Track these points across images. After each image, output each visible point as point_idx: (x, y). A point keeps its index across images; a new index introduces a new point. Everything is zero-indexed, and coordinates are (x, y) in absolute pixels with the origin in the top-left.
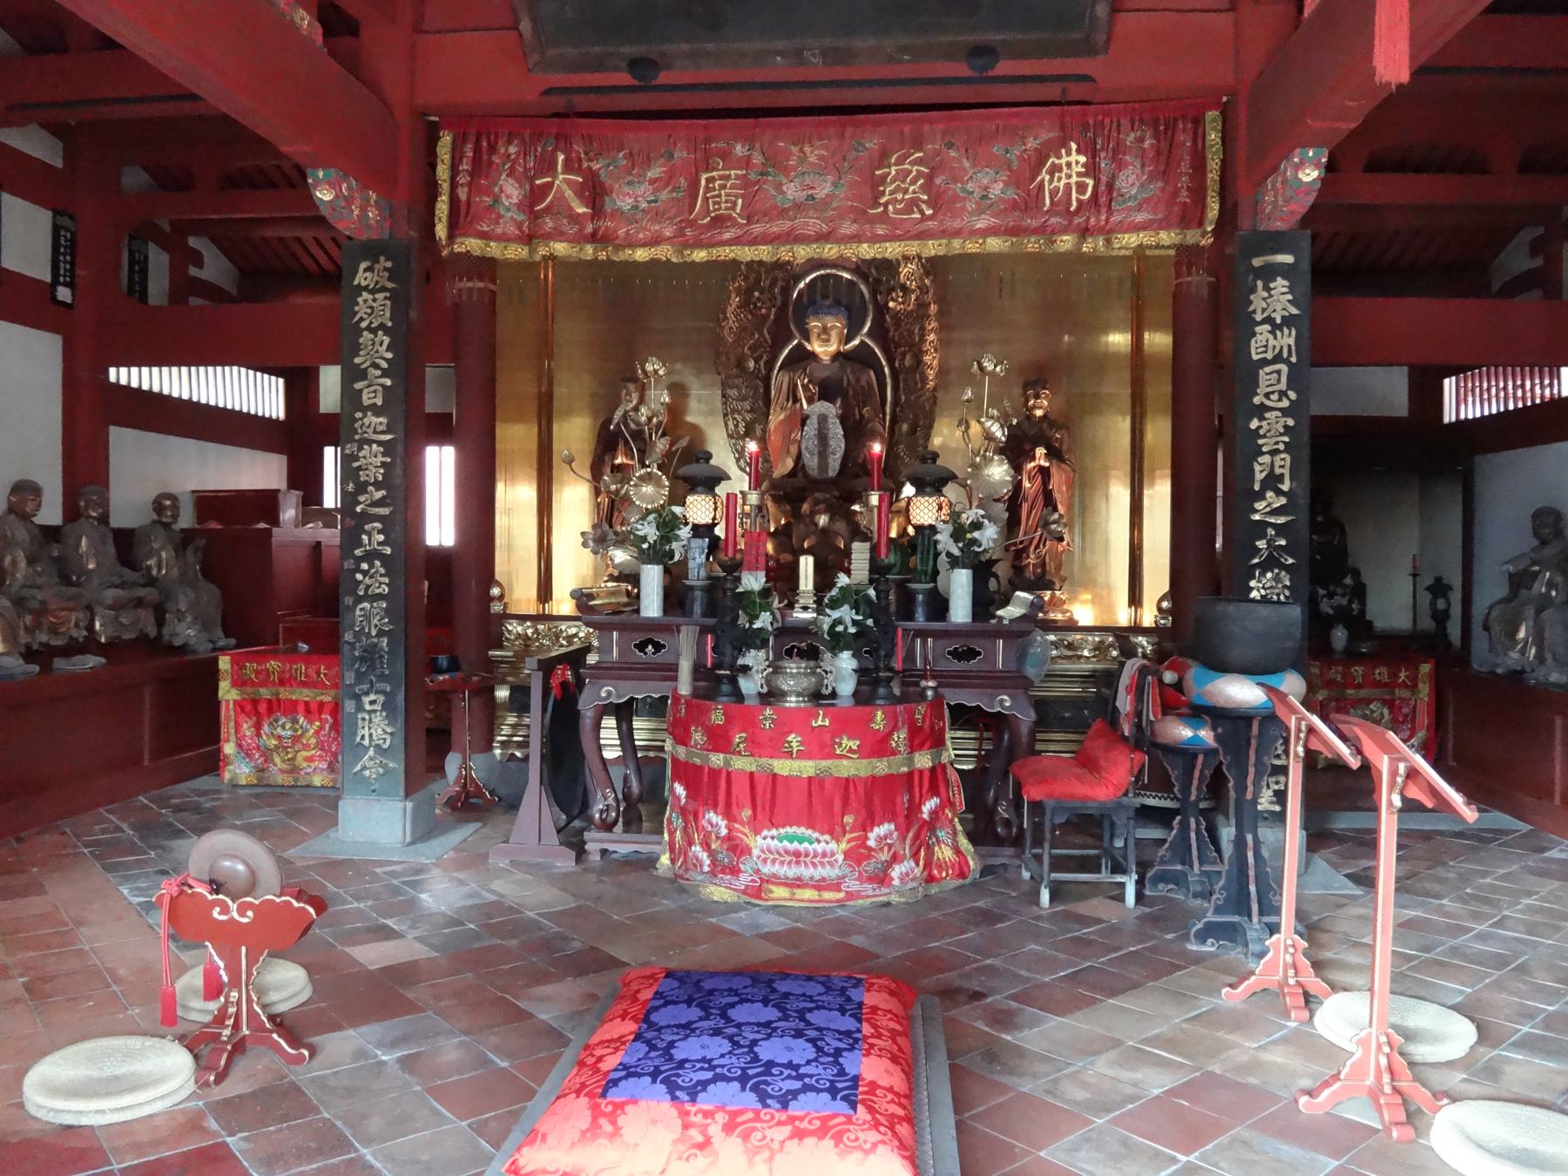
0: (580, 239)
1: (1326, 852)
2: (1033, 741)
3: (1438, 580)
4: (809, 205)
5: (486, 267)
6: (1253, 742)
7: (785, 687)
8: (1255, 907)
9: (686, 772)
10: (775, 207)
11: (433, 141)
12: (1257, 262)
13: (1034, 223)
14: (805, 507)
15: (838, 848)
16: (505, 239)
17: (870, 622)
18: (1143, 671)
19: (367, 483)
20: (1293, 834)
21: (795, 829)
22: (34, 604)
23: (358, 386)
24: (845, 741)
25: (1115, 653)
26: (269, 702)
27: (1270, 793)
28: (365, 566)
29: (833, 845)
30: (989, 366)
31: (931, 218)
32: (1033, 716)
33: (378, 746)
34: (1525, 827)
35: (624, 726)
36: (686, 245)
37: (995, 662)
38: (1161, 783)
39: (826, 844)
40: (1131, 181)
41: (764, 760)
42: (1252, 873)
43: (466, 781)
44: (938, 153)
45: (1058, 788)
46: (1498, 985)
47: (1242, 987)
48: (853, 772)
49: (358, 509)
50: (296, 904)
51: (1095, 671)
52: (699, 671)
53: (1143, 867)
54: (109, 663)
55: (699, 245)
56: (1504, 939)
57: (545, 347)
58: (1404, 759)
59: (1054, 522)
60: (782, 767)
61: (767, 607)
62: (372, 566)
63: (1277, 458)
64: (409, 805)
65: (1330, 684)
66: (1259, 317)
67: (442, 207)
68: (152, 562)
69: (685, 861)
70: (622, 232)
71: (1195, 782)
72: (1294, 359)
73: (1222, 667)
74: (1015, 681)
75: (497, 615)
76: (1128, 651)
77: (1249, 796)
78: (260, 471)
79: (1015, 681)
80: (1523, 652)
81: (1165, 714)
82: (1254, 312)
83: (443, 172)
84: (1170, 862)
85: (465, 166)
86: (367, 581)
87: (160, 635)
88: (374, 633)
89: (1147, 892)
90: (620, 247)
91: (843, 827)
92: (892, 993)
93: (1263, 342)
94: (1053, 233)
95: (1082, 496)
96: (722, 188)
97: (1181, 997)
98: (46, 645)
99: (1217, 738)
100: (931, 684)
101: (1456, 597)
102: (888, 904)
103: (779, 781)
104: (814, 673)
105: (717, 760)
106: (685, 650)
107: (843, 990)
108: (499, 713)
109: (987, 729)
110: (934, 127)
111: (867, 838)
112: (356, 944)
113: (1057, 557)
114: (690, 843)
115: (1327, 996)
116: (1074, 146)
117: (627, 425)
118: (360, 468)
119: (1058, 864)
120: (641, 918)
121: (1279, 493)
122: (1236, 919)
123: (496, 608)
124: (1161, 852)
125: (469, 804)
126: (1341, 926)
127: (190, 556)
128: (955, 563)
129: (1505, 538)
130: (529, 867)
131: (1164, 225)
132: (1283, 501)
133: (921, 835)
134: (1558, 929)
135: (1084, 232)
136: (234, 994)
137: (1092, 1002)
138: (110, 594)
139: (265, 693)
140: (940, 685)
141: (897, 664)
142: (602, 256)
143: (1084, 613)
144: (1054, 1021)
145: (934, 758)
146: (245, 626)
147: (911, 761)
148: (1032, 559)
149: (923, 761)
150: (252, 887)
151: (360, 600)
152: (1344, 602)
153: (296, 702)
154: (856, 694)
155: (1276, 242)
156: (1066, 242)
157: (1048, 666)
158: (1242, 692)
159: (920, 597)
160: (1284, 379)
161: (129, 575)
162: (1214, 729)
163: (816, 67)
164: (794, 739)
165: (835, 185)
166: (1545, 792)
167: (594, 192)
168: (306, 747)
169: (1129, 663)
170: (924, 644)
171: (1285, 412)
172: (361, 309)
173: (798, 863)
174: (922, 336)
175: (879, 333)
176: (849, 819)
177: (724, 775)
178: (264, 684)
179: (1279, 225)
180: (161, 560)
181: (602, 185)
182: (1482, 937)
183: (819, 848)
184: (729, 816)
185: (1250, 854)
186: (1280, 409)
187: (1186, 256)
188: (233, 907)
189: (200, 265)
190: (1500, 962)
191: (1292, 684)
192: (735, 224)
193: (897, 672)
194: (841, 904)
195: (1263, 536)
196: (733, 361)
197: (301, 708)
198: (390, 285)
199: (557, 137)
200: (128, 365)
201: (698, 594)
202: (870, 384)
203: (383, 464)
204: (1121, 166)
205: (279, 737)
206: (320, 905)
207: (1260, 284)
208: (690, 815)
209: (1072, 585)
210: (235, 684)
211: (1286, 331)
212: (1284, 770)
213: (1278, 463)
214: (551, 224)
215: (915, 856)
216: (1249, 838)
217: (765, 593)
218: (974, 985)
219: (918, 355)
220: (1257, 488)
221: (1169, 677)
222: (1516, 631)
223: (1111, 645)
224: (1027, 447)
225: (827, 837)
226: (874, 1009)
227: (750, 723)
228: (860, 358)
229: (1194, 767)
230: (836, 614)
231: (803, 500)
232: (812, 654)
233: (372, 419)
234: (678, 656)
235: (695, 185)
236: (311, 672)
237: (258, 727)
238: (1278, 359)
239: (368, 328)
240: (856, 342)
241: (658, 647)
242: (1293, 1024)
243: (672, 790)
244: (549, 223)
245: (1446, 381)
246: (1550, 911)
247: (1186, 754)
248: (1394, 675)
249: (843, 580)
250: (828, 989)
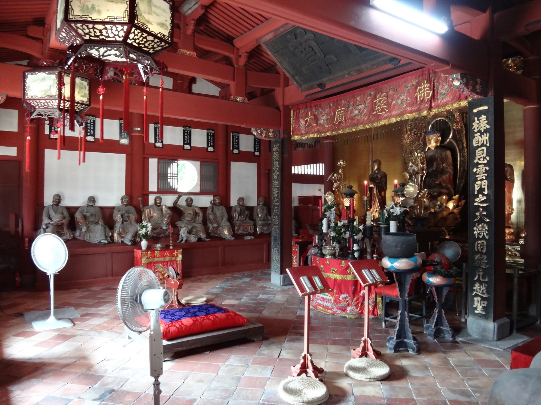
12: (475, 111)
27: (481, 307)
29: (331, 298)
63: (483, 182)
64: (282, 276)
66: (476, 131)
72: (488, 145)
82: (474, 129)
96: (339, 115)
98: (242, 233)
111: (339, 297)
121: (484, 195)
132: (485, 198)
159: (383, 229)
163: (356, 76)
171: (485, 165)
183: (328, 297)
186: (484, 164)
195: (478, 211)
207: (476, 118)
211: (485, 134)
213: (483, 183)
215: (356, 306)
220: (476, 193)
238: (483, 145)
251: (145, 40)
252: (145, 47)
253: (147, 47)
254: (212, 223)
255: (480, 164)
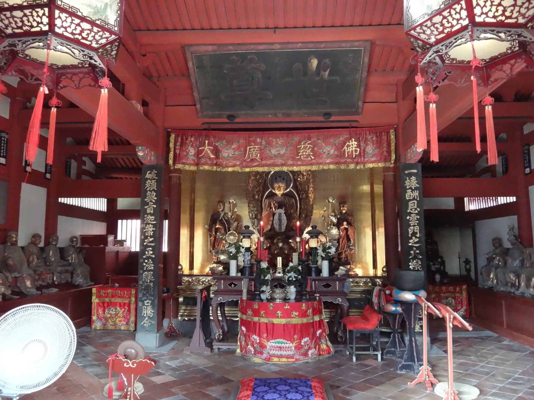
0: (212, 165)
1: (437, 344)
2: (348, 312)
3: (467, 259)
4: (276, 155)
5: (179, 171)
6: (413, 311)
7: (276, 297)
8: (416, 360)
9: (244, 323)
10: (269, 156)
11: (169, 136)
12: (406, 172)
13: (343, 161)
14: (275, 241)
15: (292, 345)
16: (190, 164)
17: (300, 277)
18: (380, 291)
19: (148, 236)
20: (426, 339)
21: (280, 340)
22: (38, 272)
23: (146, 207)
24: (294, 313)
25: (370, 284)
26: (108, 302)
27: (419, 326)
28: (146, 261)
29: (291, 345)
30: (331, 201)
31: (314, 159)
32: (348, 304)
33: (149, 317)
34: (496, 335)
35: (222, 310)
36: (243, 167)
37: (336, 289)
38: (386, 324)
39: (289, 344)
40: (370, 149)
41: (270, 319)
42: (414, 349)
43: (171, 328)
44: (315, 142)
45: (357, 325)
46: (487, 380)
47: (413, 382)
48: (296, 322)
49: (145, 244)
50: (149, 361)
51: (364, 290)
52: (249, 292)
53: (382, 350)
54: (59, 290)
55: (247, 167)
56: (488, 367)
57: (193, 191)
58: (452, 314)
59: (352, 246)
60: (276, 321)
61: (269, 273)
62: (148, 261)
63: (415, 227)
64: (158, 335)
65: (436, 292)
66: (408, 187)
67: (171, 155)
68: (69, 258)
69: (246, 351)
70: (224, 163)
71: (397, 323)
72: (418, 199)
73: (403, 289)
74: (342, 294)
75: (180, 274)
76: (374, 284)
77: (412, 327)
78: (98, 229)
79: (342, 294)
80: (492, 281)
81: (387, 303)
83: (172, 145)
84: (391, 348)
85: (178, 144)
86: (147, 265)
87: (72, 281)
88: (148, 281)
89: (384, 357)
90: (224, 167)
91: (294, 339)
92: (318, 383)
93: (409, 195)
94: (349, 163)
95: (358, 237)
96: (254, 151)
97: (396, 386)
98: (41, 285)
99: (403, 310)
100: (318, 295)
101: (473, 265)
102: (307, 362)
103: (275, 325)
104: (284, 292)
105: (256, 319)
106: (244, 286)
107: (305, 382)
108: (180, 306)
109: (333, 308)
110: (314, 134)
111: (301, 342)
112: (151, 376)
113: (351, 255)
114: (247, 345)
115: (437, 383)
116: (353, 139)
117: (224, 218)
118: (146, 232)
119: (358, 349)
120: (234, 368)
121: (416, 237)
122: (410, 363)
123: (180, 273)
124: (387, 345)
125: (171, 335)
126: (441, 365)
127: (81, 256)
128: (323, 259)
129: (485, 248)
130: (197, 354)
131: (379, 161)
132: (418, 240)
133: (317, 341)
134: (504, 364)
135: (357, 163)
136: (130, 389)
137: (371, 388)
138: (59, 269)
139: (107, 300)
140: (320, 295)
141: (308, 289)
142: (219, 170)
143: (359, 272)
144: (361, 393)
145: (320, 317)
146: (96, 278)
147: (313, 318)
148: (344, 256)
149: (317, 318)
150: (136, 357)
151: (144, 271)
152: (438, 267)
153: (117, 303)
154: (295, 299)
155: (411, 166)
156: (352, 166)
157: (351, 289)
158: (409, 296)
159: (313, 269)
160: (416, 205)
161: (65, 263)
162: (401, 307)
163: (280, 117)
164: (279, 312)
165: (286, 150)
166: (501, 324)
167: (217, 152)
168: (119, 317)
169: (376, 288)
170: (315, 283)
171: (417, 214)
172: (147, 185)
173: (281, 350)
174: (308, 189)
175: (295, 187)
176: (296, 337)
177: (258, 324)
178: (107, 297)
179: (413, 162)
180: (73, 258)
181: (219, 150)
182: (482, 367)
183: (287, 345)
184: (259, 336)
185: (414, 344)
187: (386, 169)
188: (130, 362)
189: (85, 165)
190: (487, 373)
191: (423, 294)
192: (257, 161)
193: (308, 292)
194: (294, 362)
195: (412, 250)
196: (251, 196)
197: (118, 304)
198: (156, 178)
199: (206, 136)
200: (64, 197)
201: (247, 268)
202: (293, 203)
203: (153, 231)
204: (367, 145)
205: (111, 314)
206: (155, 362)
207: (407, 178)
208: (247, 337)
209: (356, 263)
210: (97, 297)
212: (421, 319)
213: (415, 229)
214: (204, 161)
215: (315, 348)
216: (413, 339)
217: (268, 268)
218: (337, 384)
219: (307, 193)
221: (388, 292)
222: (490, 275)
223: (369, 282)
224: (341, 222)
225: (289, 342)
226: (315, 387)
227: (266, 308)
228: (289, 195)
229: (396, 319)
230: (289, 275)
231: (274, 238)
232: (282, 287)
233: (150, 217)
234: (241, 287)
235: (246, 150)
236: (122, 293)
237: (104, 311)
238: (414, 199)
239: (149, 190)
240: (288, 190)
241: (235, 285)
242: (428, 392)
243: (241, 329)
244: (203, 160)
245: (465, 198)
246: (502, 359)
247: (394, 315)
248: (455, 289)
249: (291, 264)
250: (301, 382)
251: (501, 9)
252: (507, 18)
253: (510, 17)
254: (10, 271)
255: (413, 213)
